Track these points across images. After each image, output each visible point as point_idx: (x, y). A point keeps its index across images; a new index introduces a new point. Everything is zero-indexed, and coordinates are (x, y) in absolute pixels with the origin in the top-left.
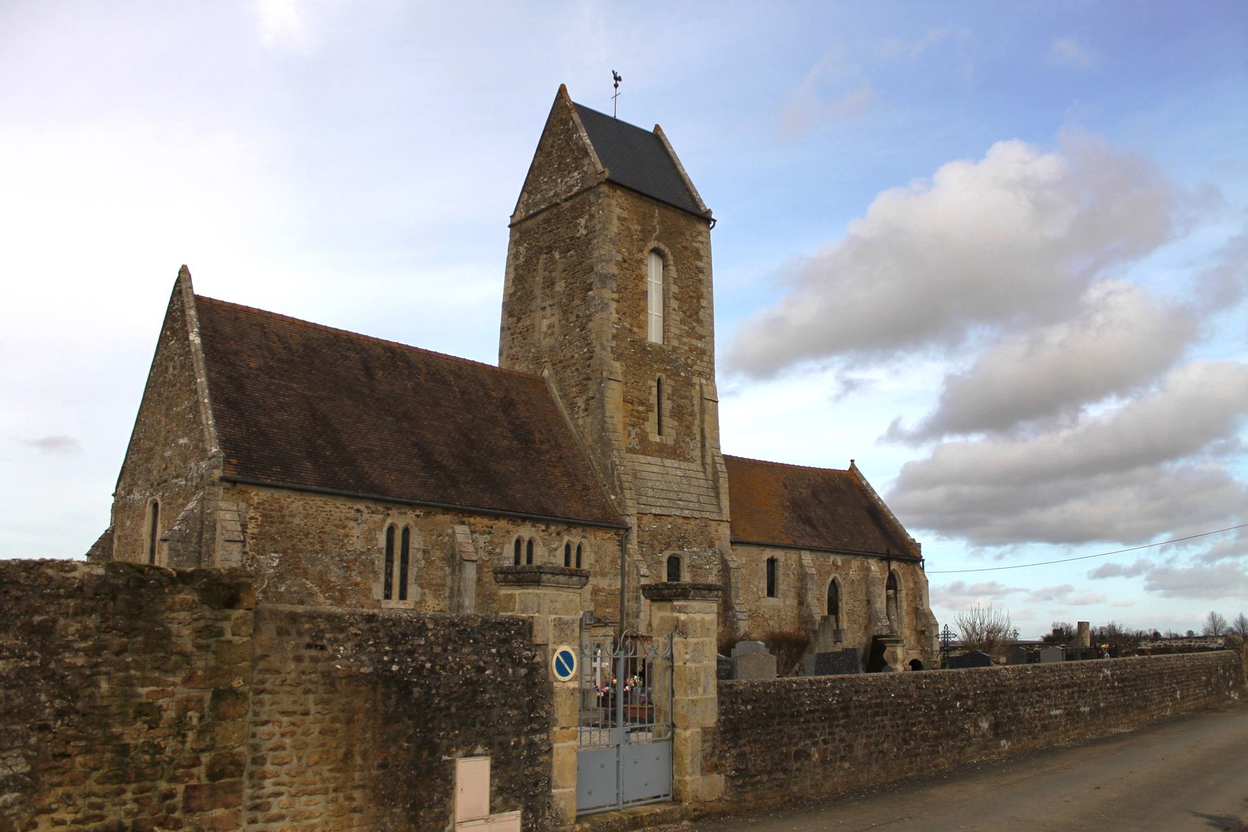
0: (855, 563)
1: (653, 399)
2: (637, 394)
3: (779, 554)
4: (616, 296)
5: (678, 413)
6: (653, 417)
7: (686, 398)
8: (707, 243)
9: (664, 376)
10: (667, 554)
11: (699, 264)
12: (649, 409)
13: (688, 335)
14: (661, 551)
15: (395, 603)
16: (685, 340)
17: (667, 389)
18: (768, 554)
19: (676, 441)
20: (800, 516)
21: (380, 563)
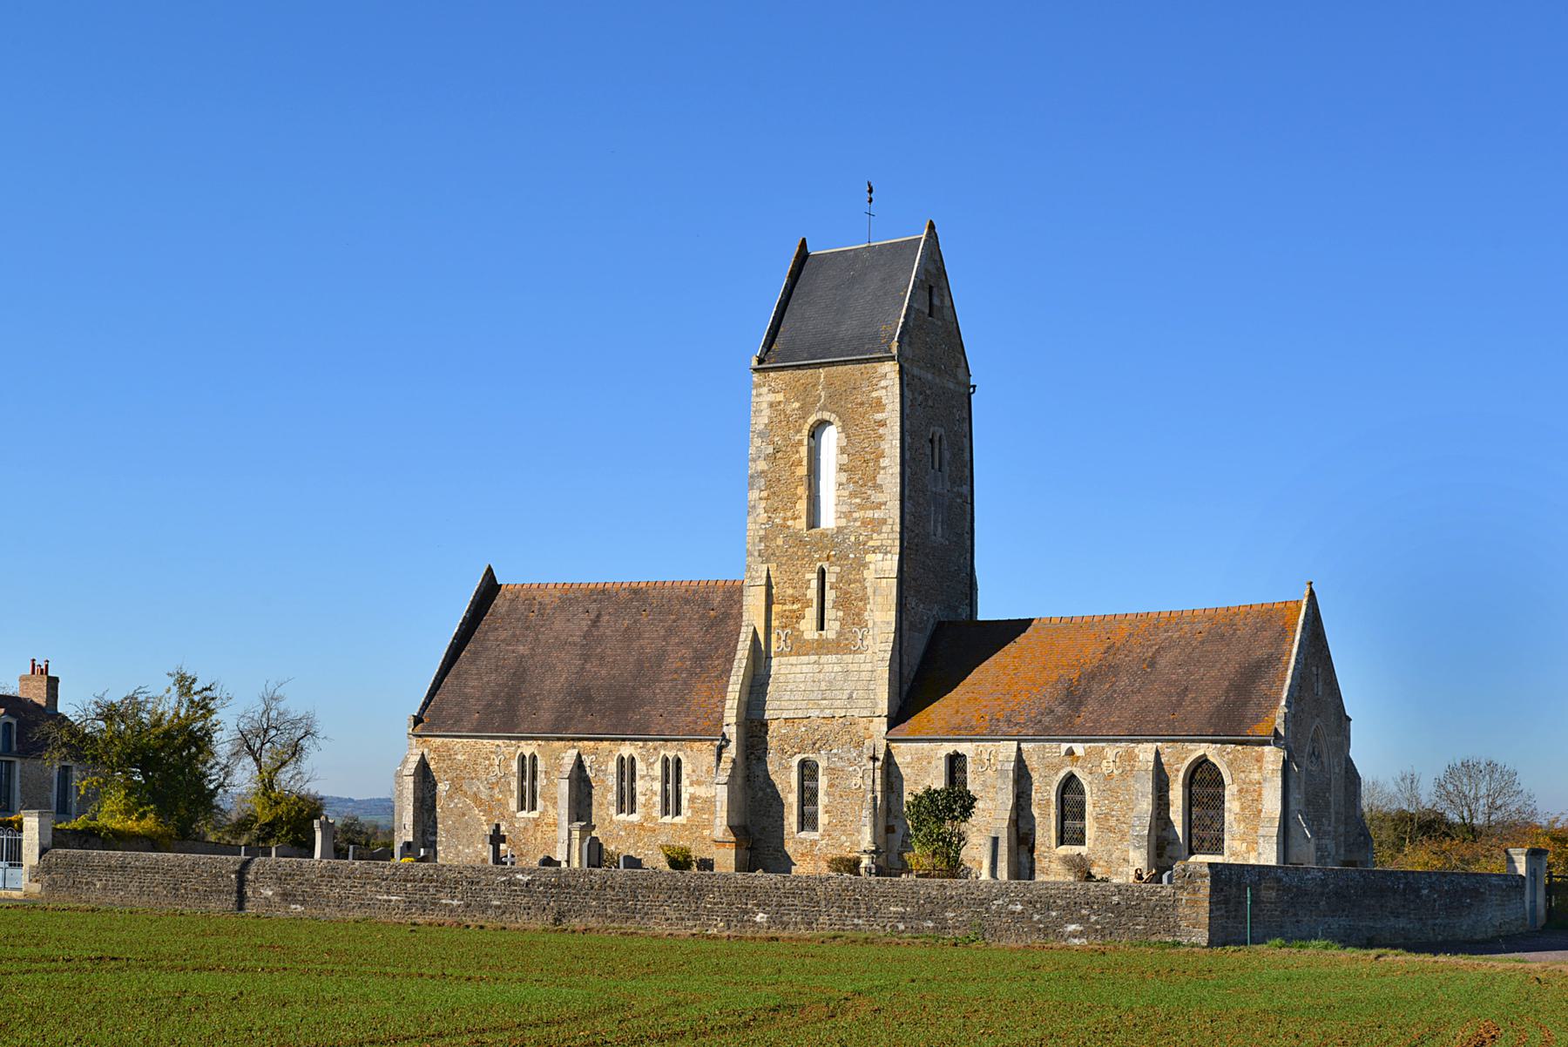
0: (1111, 751)
1: (812, 593)
2: (790, 591)
3: (962, 748)
4: (764, 494)
5: (843, 602)
6: (811, 613)
7: (855, 581)
8: (570, 598)
9: (826, 566)
10: (797, 758)
11: (879, 416)
12: (808, 604)
13: (861, 507)
14: (791, 756)
15: (671, 755)
16: (856, 515)
17: (830, 579)
18: (949, 748)
19: (840, 634)
20: (1114, 669)
21: (514, 785)
